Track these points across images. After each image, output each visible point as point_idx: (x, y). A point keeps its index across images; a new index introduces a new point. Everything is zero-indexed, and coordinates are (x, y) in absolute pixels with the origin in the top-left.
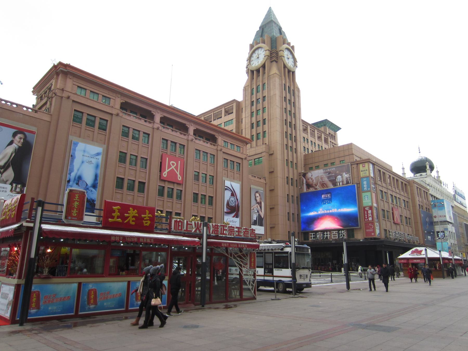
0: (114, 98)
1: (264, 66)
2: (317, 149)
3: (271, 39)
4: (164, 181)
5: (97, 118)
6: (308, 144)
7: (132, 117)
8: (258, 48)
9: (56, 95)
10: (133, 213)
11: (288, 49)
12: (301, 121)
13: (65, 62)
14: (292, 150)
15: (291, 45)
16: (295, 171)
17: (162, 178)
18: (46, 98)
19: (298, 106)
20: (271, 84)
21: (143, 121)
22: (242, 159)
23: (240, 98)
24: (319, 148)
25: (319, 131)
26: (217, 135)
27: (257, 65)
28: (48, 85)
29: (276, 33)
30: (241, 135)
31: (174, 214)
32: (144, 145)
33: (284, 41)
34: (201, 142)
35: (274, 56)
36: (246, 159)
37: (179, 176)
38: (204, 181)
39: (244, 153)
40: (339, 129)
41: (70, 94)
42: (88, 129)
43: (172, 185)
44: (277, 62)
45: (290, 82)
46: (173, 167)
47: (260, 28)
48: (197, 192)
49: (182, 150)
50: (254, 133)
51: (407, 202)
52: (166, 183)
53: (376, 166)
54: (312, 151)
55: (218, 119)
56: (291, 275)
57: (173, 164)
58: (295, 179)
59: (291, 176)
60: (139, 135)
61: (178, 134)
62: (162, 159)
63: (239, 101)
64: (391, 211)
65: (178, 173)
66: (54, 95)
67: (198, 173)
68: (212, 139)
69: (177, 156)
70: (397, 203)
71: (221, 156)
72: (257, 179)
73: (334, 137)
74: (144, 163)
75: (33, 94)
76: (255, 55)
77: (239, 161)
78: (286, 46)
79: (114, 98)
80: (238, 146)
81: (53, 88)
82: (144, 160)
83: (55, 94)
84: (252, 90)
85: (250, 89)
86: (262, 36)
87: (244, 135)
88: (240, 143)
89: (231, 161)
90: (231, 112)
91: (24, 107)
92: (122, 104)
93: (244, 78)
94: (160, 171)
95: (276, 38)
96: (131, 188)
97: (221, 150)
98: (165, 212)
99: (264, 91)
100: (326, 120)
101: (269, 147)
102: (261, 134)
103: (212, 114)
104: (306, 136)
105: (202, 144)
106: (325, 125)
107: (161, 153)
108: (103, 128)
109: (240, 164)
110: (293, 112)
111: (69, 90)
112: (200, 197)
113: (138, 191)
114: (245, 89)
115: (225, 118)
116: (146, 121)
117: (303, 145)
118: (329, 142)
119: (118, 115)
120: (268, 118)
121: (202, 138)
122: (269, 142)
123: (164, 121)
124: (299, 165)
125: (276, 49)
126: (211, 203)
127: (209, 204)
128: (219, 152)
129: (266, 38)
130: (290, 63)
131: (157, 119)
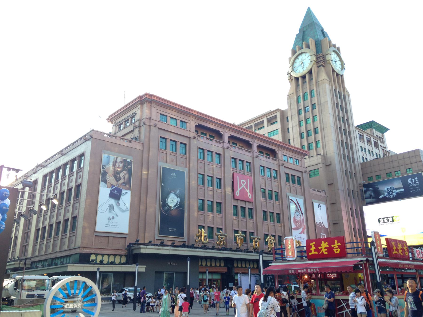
1: (310, 72)
2: (375, 157)
6: (363, 152)
8: (301, 54)
10: (324, 245)
11: (334, 51)
15: (337, 46)
16: (355, 181)
17: (235, 198)
20: (321, 91)
22: (302, 172)
23: (284, 106)
24: (377, 156)
27: (302, 71)
29: (320, 36)
32: (171, 154)
35: (321, 60)
36: (305, 172)
37: (249, 194)
38: (201, 183)
40: (387, 130)
43: (244, 203)
44: (324, 66)
45: (335, 84)
46: (243, 186)
47: (300, 30)
56: (21, 298)
58: (356, 190)
59: (351, 188)
65: (248, 191)
68: (272, 153)
71: (283, 171)
72: (316, 193)
73: (382, 140)
76: (298, 61)
78: (332, 49)
84: (298, 98)
88: (298, 156)
91: (104, 134)
93: (287, 87)
95: (321, 41)
96: (211, 209)
97: (283, 165)
99: (313, 99)
100: (372, 121)
101: (325, 158)
103: (253, 124)
105: (264, 160)
106: (371, 127)
107: (232, 172)
112: (268, 214)
114: (289, 97)
118: (380, 147)
120: (321, 127)
124: (358, 175)
128: (281, 167)
130: (337, 67)
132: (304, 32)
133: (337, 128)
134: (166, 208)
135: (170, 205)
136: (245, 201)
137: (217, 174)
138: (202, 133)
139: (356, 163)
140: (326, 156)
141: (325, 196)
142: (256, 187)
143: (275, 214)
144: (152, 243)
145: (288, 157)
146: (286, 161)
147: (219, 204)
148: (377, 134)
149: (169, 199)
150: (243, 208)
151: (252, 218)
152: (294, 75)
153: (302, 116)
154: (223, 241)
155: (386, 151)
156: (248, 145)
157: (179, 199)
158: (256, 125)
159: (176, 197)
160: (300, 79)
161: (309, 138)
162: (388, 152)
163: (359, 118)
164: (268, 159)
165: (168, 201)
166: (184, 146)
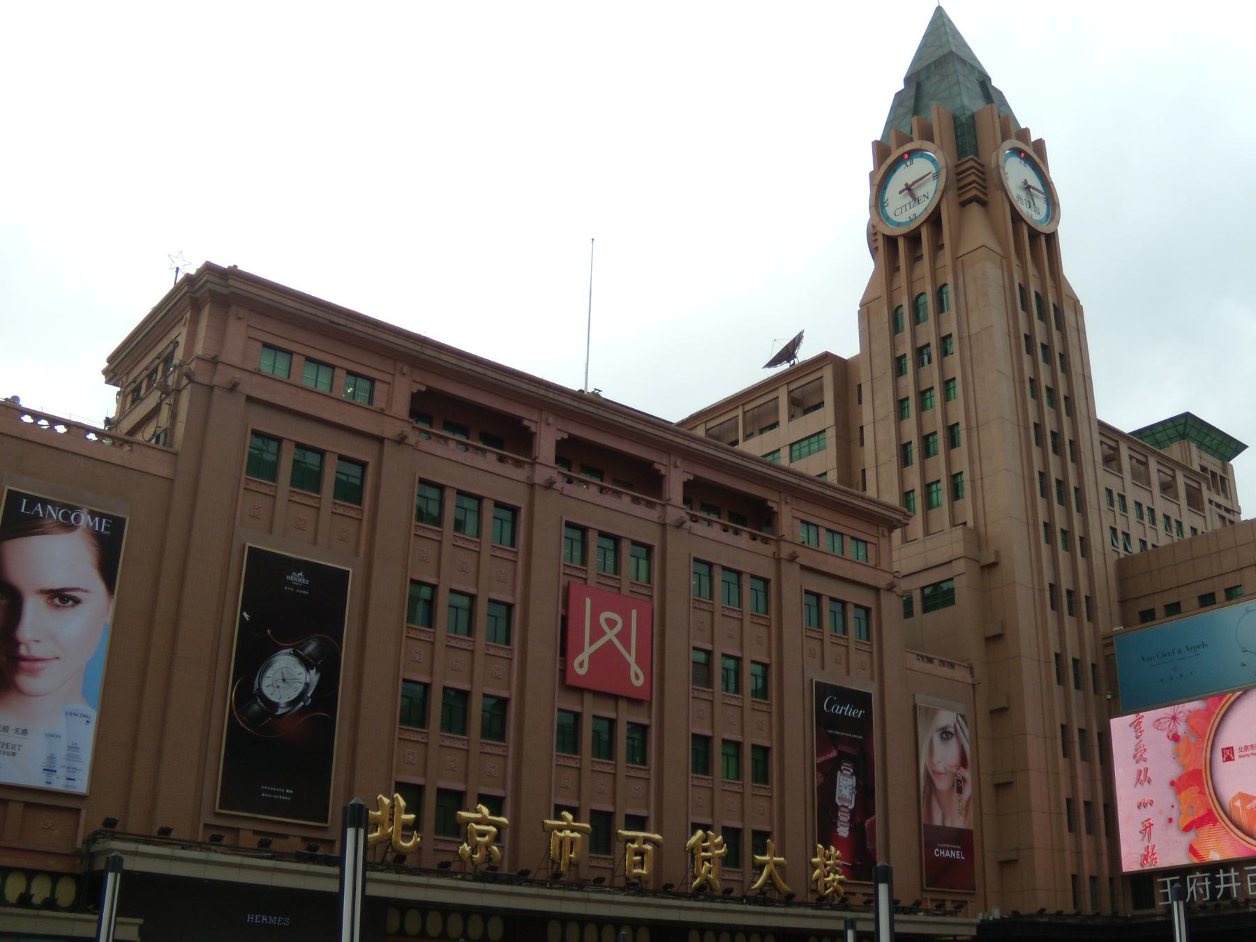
0: (388, 378)
1: (934, 220)
3: (955, 118)
4: (580, 691)
5: (328, 456)
6: (1126, 518)
7: (452, 445)
9: (191, 381)
11: (1017, 151)
12: (1095, 427)
13: (224, 263)
14: (1068, 545)
18: (157, 394)
21: (493, 458)
25: (1164, 460)
26: (773, 499)
28: (160, 348)
30: (861, 493)
31: (620, 819)
33: (1008, 127)
34: (715, 532)
36: (890, 588)
37: (634, 668)
39: (884, 564)
40: (1239, 447)
41: (238, 375)
42: (296, 498)
44: (983, 204)
46: (611, 635)
47: (907, 80)
48: (708, 733)
50: (914, 480)
54: (1143, 543)
55: (762, 431)
58: (1089, 660)
59: (1071, 652)
60: (441, 503)
62: (566, 605)
63: (846, 357)
65: (631, 659)
66: (185, 381)
67: (709, 653)
68: (751, 514)
69: (625, 590)
71: (793, 585)
73: (1223, 483)
74: (502, 624)
75: (108, 382)
77: (866, 599)
79: (388, 378)
80: (857, 540)
81: (179, 355)
82: (502, 611)
83: (188, 376)
85: (885, 310)
86: (916, 110)
87: (871, 492)
89: (832, 599)
90: (817, 402)
92: (416, 397)
93: (860, 267)
94: (563, 652)
95: (973, 117)
97: (793, 558)
98: (585, 813)
101: (977, 538)
102: (944, 485)
103: (740, 412)
104: (1113, 483)
107: (564, 581)
108: (350, 492)
109: (867, 610)
110: (1062, 392)
111: (236, 360)
115: (790, 430)
116: (502, 459)
117: (1108, 522)
119: (401, 441)
121: (717, 512)
122: (975, 518)
123: (572, 454)
124: (1100, 601)
125: (976, 153)
126: (762, 775)
127: (756, 779)
128: (784, 565)
129: (935, 115)
131: (546, 447)
132: (919, 87)
133: (1027, 428)
134: (256, 707)
135: (274, 698)
137: (495, 584)
139: (1097, 560)
140: (982, 529)
141: (970, 680)
142: (667, 641)
143: (747, 753)
145: (822, 531)
148: (1204, 463)
149: (270, 673)
151: (644, 761)
153: (908, 381)
154: (487, 846)
155: (1232, 522)
157: (313, 677)
159: (301, 669)
160: (901, 243)
161: (930, 461)
164: (758, 544)
165: (266, 682)
166: (507, 515)
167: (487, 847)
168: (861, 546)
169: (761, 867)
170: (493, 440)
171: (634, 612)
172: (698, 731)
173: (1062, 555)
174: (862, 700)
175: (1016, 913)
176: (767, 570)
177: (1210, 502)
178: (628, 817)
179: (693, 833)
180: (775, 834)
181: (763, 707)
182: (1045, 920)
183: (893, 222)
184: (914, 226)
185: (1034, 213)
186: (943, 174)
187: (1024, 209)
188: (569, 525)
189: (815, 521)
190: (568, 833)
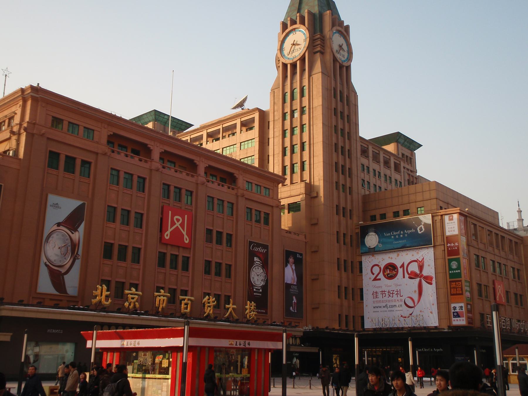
0: (99, 130)
11: (339, 32)
12: (358, 139)
19: (354, 121)
31: (179, 292)
35: (317, 44)
37: (186, 236)
45: (342, 84)
46: (178, 224)
49: (189, 198)
51: (518, 270)
52: (169, 248)
53: (469, 219)
57: (178, 220)
61: (184, 175)
62: (162, 213)
64: (491, 286)
65: (185, 233)
69: (183, 208)
70: (501, 273)
71: (242, 204)
73: (411, 160)
79: (99, 130)
87: (271, 170)
93: (273, 74)
94: (161, 231)
96: (122, 257)
98: (167, 289)
113: (65, 170)
115: (241, 135)
118: (402, 169)
123: (211, 171)
126: (229, 275)
128: (240, 198)
136: (179, 247)
138: (120, 146)
140: (312, 183)
144: (23, 303)
145: (254, 185)
146: (250, 190)
147: (229, 236)
148: (404, 152)
150: (175, 258)
152: (282, 60)
155: (413, 176)
156: (190, 165)
158: (209, 135)
162: (416, 178)
163: (371, 125)
164: (230, 190)
167: (134, 303)
168: (267, 190)
169: (228, 309)
170: (136, 152)
171: (186, 216)
172: (207, 259)
173: (342, 194)
174: (265, 247)
175: (317, 328)
176: (233, 200)
177: (404, 168)
178: (182, 290)
179: (204, 297)
180: (232, 296)
181: (259, 226)
182: (328, 331)
183: (286, 58)
184: (295, 60)
185: (341, 57)
186: (308, 40)
187: (338, 56)
188: (164, 184)
189: (251, 181)
190: (162, 297)
